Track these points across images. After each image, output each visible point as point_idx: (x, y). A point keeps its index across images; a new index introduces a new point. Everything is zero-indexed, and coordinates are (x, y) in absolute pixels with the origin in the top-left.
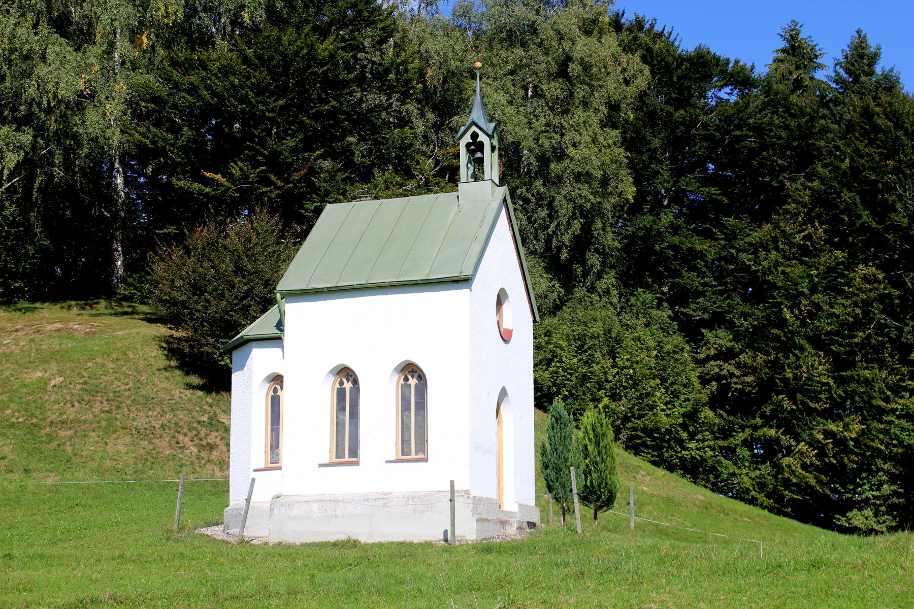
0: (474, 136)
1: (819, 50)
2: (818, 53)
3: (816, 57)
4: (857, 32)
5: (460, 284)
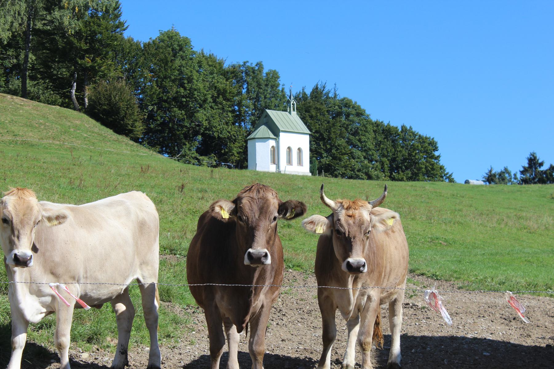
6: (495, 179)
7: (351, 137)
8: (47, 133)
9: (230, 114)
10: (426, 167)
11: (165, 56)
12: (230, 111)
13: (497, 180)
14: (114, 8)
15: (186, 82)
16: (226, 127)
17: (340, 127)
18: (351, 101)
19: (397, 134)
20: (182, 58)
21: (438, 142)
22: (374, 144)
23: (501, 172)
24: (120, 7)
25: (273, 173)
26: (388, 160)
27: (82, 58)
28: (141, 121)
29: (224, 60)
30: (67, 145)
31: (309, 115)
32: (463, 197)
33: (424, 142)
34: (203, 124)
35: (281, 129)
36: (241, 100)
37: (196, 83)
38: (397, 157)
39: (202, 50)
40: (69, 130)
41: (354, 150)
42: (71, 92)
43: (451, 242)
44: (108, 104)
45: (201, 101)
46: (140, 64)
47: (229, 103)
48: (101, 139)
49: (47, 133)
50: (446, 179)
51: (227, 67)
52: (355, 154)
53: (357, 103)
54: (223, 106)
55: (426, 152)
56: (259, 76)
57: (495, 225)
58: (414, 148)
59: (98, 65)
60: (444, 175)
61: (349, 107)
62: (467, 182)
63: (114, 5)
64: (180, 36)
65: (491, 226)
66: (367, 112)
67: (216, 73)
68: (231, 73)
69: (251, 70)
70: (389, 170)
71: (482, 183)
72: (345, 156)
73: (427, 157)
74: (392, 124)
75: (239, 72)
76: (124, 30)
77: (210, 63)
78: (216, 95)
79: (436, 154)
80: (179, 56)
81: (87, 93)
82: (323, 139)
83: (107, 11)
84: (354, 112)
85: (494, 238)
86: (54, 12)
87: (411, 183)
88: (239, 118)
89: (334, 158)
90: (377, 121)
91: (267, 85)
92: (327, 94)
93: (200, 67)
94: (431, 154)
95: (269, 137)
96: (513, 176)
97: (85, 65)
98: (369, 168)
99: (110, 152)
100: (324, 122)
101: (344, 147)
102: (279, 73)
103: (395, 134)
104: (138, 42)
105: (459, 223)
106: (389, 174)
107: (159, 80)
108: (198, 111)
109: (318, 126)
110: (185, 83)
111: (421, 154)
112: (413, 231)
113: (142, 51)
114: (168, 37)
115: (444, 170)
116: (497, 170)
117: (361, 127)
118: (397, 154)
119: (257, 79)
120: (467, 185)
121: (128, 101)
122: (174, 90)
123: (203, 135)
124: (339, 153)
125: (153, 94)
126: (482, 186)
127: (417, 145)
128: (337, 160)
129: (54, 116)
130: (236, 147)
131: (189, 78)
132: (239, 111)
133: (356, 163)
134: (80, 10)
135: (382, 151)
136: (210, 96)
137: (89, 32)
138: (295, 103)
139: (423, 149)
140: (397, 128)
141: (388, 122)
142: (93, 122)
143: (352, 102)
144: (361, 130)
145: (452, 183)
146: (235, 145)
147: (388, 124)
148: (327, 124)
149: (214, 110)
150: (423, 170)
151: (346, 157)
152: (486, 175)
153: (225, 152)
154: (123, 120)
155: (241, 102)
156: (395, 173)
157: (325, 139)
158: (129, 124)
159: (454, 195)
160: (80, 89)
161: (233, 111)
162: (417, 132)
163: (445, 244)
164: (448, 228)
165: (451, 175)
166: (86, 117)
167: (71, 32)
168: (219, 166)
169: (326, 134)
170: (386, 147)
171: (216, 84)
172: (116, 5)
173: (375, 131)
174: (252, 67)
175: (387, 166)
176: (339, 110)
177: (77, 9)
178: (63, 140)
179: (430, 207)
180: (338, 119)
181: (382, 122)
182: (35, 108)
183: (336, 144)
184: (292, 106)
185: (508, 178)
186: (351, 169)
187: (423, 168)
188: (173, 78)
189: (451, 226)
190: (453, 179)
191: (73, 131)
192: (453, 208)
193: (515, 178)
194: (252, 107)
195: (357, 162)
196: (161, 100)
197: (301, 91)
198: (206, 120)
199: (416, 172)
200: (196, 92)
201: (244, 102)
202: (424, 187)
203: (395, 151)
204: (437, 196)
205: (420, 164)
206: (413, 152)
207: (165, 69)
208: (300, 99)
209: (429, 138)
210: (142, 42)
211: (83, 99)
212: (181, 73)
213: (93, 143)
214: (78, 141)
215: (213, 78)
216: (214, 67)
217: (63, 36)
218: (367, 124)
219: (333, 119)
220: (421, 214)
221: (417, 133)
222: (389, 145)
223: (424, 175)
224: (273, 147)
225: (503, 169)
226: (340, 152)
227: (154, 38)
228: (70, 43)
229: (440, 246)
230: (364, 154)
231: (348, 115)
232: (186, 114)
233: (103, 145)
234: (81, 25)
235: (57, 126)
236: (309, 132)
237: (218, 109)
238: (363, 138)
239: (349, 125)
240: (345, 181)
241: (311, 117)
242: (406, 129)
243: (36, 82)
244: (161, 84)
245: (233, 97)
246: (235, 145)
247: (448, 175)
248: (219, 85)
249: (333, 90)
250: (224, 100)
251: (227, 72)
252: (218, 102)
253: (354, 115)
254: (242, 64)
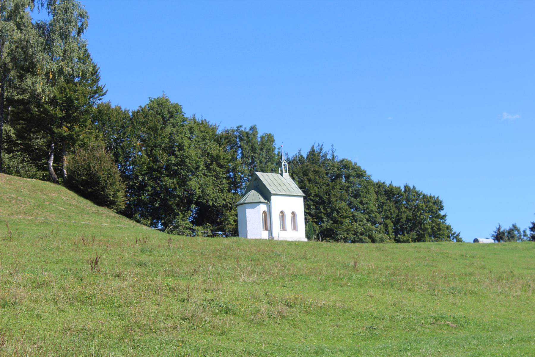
6: (504, 237)
7: (352, 199)
8: (19, 208)
9: (224, 181)
10: (432, 228)
11: (155, 123)
12: (224, 178)
13: (506, 238)
14: (91, 73)
15: (176, 149)
16: (220, 194)
17: (341, 189)
18: (350, 162)
19: (400, 195)
20: (173, 125)
21: (443, 201)
22: (377, 206)
23: (510, 229)
24: (99, 71)
25: (266, 240)
26: (392, 222)
27: (60, 126)
28: (123, 191)
29: (217, 125)
30: (39, 220)
31: (307, 179)
32: (473, 257)
33: (429, 201)
34: (196, 193)
35: (272, 192)
36: (236, 166)
37: (188, 150)
38: (402, 218)
39: (194, 116)
40: (43, 203)
41: (355, 213)
42: (48, 164)
43: (462, 323)
44: (87, 174)
45: (194, 168)
46: (128, 132)
47: (223, 170)
48: (79, 212)
49: (19, 208)
50: (453, 239)
51: (220, 132)
52: (357, 217)
53: (356, 164)
54: (217, 173)
55: (431, 211)
56: (254, 140)
57: (519, 293)
58: (417, 208)
59: (76, 133)
60: (452, 235)
61: (348, 168)
62: (476, 241)
63: (91, 69)
64: (170, 102)
65: (515, 294)
66: (368, 173)
67: (209, 139)
68: (225, 139)
69: (245, 134)
70: (393, 232)
71: (493, 241)
72: (346, 219)
73: (433, 217)
74: (395, 184)
75: (234, 136)
76: (103, 95)
77: (202, 129)
78: (209, 162)
79: (442, 213)
80: (169, 123)
81: (65, 164)
82: (323, 203)
83: (84, 76)
84: (354, 173)
85: (520, 313)
86: (26, 79)
87: (417, 244)
88: (234, 184)
89: (335, 221)
90: (379, 182)
91: (262, 149)
92: (325, 155)
93: (191, 133)
94: (437, 213)
95: (258, 201)
96: (522, 234)
97: (62, 134)
98: (372, 230)
99: (87, 226)
100: (323, 185)
101: (345, 210)
102: (274, 137)
103: (398, 194)
104: (126, 110)
105: (472, 293)
106: (394, 236)
107: (149, 149)
108: (191, 179)
109: (317, 190)
110: (176, 151)
111: (426, 214)
112: (410, 308)
113: (131, 119)
114: (158, 104)
115: (451, 230)
116: (506, 227)
117: (362, 189)
118: (401, 215)
119: (251, 143)
120: (476, 243)
121: (109, 170)
122: (164, 158)
123: (197, 204)
124: (340, 216)
125: (143, 163)
126: (492, 244)
127: (421, 205)
128: (338, 224)
129: (28, 190)
130: (232, 215)
131: (180, 145)
132: (235, 177)
133: (358, 226)
134: (54, 76)
135: (385, 212)
136: (203, 163)
137: (65, 99)
138: (286, 163)
139: (427, 209)
140: (399, 188)
141: (390, 183)
142: (72, 194)
143: (352, 163)
144: (362, 192)
145: (460, 243)
146: (231, 213)
147: (391, 185)
148: (327, 187)
149: (207, 177)
150: (430, 230)
151: (347, 221)
152: (494, 234)
153: (220, 220)
154: (104, 191)
155: (236, 168)
156: (400, 235)
157: (325, 202)
158: (110, 195)
159: (462, 256)
160: (58, 160)
161: (228, 178)
162: (420, 192)
163: (455, 325)
164: (458, 301)
165: (458, 235)
166: (63, 189)
167: (44, 99)
168: (215, 236)
169: (326, 198)
170: (389, 208)
171: (208, 151)
172: (93, 70)
173: (377, 193)
174: (246, 131)
175: (391, 228)
176: (339, 172)
177: (51, 75)
178: (36, 214)
179: (434, 272)
180: (338, 181)
181: (384, 183)
182: (8, 182)
183: (337, 208)
184: (283, 167)
185: (518, 235)
186: (353, 233)
187: (428, 229)
188: (163, 145)
189: (461, 298)
190: (461, 238)
191: (48, 204)
192: (463, 271)
193: (525, 235)
194: (247, 172)
195: (360, 225)
196: (150, 169)
197: (298, 154)
198: (199, 188)
199: (422, 233)
200: (187, 160)
201: (239, 168)
202: (429, 248)
203: (399, 212)
204: (444, 258)
205: (426, 225)
206: (418, 212)
207: (155, 137)
208: (297, 162)
209: (434, 197)
210: (131, 111)
211: (62, 170)
212: (171, 139)
213: (70, 216)
214: (52, 216)
215: (206, 144)
216: (207, 133)
217: (39, 105)
218: (368, 185)
219: (332, 182)
220: (421, 283)
221: (421, 193)
222: (392, 206)
223: (430, 235)
224: (264, 212)
225: (511, 227)
226: (342, 215)
227: (143, 106)
228: (46, 111)
229: (447, 329)
230: (367, 217)
231: (348, 177)
232: (177, 183)
233: (80, 218)
234: (55, 92)
235: (30, 200)
236: (303, 195)
237: (212, 176)
238: (365, 200)
239: (350, 187)
240: (349, 245)
241: (310, 180)
242: (409, 189)
243: (11, 155)
244: (151, 153)
245: (228, 163)
246: (231, 213)
247: (455, 235)
248: (211, 151)
249: (331, 151)
250: (218, 166)
251: (221, 138)
252: (211, 169)
253: (354, 176)
254: (236, 129)
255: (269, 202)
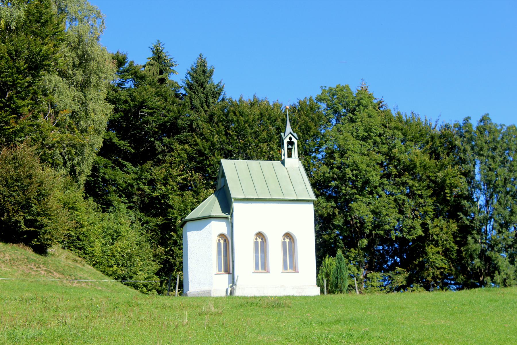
0: (290, 139)
1: (174, 62)
2: (174, 63)
3: (172, 66)
4: (200, 55)
5: (309, 202)
255: (229, 217)
